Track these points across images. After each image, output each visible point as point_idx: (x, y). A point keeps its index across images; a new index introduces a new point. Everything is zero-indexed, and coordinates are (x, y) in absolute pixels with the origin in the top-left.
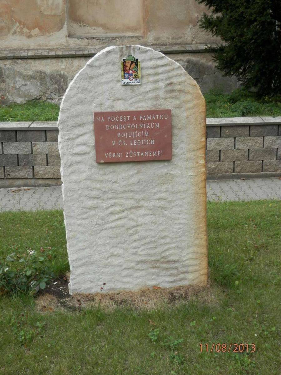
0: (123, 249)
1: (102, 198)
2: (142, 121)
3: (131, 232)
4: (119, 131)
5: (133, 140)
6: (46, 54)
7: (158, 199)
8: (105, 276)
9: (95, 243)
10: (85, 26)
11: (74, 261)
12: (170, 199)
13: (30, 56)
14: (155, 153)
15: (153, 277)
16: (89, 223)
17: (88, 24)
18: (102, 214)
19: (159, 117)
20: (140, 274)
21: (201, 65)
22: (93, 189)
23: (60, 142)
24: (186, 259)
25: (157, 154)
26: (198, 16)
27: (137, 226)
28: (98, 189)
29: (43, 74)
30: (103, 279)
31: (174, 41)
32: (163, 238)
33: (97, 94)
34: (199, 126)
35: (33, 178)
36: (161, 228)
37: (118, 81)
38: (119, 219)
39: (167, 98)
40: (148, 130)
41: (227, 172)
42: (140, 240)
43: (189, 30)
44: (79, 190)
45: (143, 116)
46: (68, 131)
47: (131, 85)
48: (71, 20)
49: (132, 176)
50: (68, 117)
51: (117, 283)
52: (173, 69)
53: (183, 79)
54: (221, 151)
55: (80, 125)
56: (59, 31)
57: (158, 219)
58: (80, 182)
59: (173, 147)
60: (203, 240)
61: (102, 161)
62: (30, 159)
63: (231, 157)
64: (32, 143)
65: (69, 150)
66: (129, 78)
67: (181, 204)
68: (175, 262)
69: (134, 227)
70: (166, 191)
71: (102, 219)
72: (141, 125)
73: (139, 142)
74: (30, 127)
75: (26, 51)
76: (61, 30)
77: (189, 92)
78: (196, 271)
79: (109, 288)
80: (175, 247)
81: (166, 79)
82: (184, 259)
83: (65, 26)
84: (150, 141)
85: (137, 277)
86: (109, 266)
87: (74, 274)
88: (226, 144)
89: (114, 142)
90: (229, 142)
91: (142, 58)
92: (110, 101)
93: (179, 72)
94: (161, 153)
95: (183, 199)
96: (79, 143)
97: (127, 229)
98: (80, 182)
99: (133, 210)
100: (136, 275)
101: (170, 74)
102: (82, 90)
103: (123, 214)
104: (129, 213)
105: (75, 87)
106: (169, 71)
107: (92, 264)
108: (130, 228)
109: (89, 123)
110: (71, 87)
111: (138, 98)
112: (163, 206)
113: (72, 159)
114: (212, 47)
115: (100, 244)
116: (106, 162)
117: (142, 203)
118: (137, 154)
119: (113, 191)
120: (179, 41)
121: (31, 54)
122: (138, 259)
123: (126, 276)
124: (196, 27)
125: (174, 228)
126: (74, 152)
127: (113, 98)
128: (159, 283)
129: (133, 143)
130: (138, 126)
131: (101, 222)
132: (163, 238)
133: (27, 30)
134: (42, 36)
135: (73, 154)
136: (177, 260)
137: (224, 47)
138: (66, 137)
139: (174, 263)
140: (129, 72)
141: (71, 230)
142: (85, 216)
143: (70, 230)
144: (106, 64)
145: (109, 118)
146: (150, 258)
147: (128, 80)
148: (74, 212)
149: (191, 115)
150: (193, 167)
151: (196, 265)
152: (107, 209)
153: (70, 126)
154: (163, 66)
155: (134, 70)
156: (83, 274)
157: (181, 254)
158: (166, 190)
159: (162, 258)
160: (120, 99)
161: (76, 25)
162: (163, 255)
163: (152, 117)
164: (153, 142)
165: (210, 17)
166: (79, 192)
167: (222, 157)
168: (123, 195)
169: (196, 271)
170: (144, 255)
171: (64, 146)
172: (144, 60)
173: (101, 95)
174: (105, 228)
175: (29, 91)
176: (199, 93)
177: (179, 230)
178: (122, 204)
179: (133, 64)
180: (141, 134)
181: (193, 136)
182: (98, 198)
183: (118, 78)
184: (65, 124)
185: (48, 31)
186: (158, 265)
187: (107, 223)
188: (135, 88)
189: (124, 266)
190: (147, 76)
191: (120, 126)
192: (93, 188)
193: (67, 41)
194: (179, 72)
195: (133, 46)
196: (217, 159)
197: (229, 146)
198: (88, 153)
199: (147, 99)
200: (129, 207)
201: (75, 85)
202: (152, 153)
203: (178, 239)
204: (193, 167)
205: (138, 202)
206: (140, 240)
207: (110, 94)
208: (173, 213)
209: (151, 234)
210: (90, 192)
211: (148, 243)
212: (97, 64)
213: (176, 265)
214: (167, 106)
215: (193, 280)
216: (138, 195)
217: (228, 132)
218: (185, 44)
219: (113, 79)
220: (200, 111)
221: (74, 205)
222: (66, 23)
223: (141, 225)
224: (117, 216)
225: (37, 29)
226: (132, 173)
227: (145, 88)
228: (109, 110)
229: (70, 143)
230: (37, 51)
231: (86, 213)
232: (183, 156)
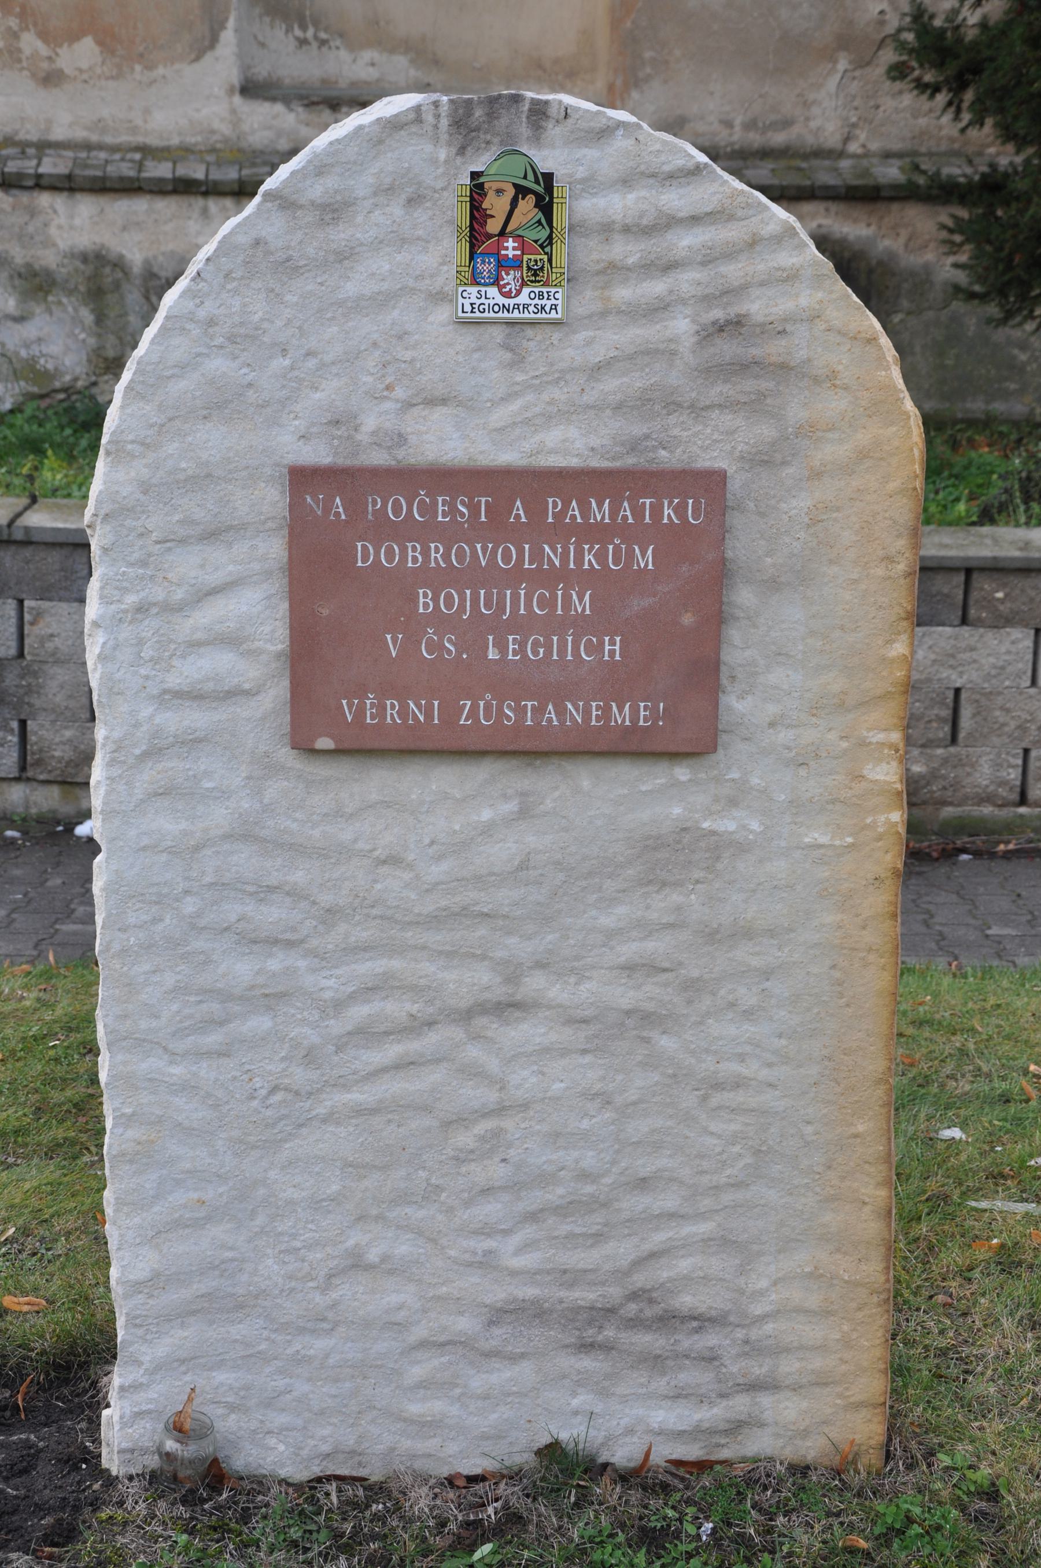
0: (420, 1233)
1: (314, 942)
2: (561, 531)
3: (465, 1139)
4: (428, 577)
5: (500, 629)
6: (127, 170)
7: (629, 968)
8: (309, 1380)
9: (262, 1191)
10: (323, 43)
11: (136, 1287)
12: (695, 973)
13: (51, 175)
14: (621, 710)
15: (575, 1402)
16: (235, 1078)
17: (341, 35)
18: (312, 1036)
19: (657, 511)
20: (500, 1375)
21: (880, 263)
22: (265, 892)
23: (96, 624)
24: (768, 1308)
25: (634, 718)
26: (882, 12)
27: (500, 1110)
28: (295, 894)
29: (107, 270)
30: (295, 1394)
31: (756, 140)
32: (643, 1184)
33: (311, 363)
34: (880, 572)
35: (17, 779)
36: (639, 1127)
37: (440, 297)
38: (403, 1065)
39: (707, 408)
40: (586, 579)
41: (988, 799)
42: (515, 1187)
43: (832, 83)
44: (187, 892)
45: (566, 505)
46: (143, 563)
47: (511, 324)
48: (257, 11)
49: (487, 830)
50: (146, 487)
51: (373, 1421)
52: (753, 243)
53: (806, 298)
54: (964, 695)
55: (212, 535)
56: (197, 59)
57: (619, 1077)
58: (197, 848)
59: (724, 681)
60: (867, 1209)
61: (325, 743)
62: (8, 682)
63: (1013, 724)
64: (21, 602)
65: (143, 671)
66: (496, 282)
67: (753, 1001)
68: (701, 1321)
69: (486, 1114)
70: (671, 926)
71: (310, 1057)
72: (554, 550)
73: (536, 644)
74: (19, 522)
75: (31, 151)
76: (208, 57)
77: (832, 376)
78: (822, 1381)
79: (325, 1448)
80: (707, 1241)
81: (707, 300)
82: (758, 1309)
83: (228, 36)
84: (601, 643)
85: (486, 1397)
86: (336, 1324)
87: (139, 1363)
88: (992, 660)
89: (395, 640)
90: (1009, 652)
91: (581, 172)
92: (388, 405)
93: (786, 259)
94: (654, 716)
95: (767, 974)
96: (199, 635)
97: (447, 1125)
98: (197, 848)
99: (480, 1021)
100: (477, 1382)
101: (733, 271)
102: (232, 339)
103: (430, 1041)
104: (457, 1033)
105: (191, 318)
106: (729, 254)
107: (241, 1307)
108: (460, 1121)
109: (264, 523)
110: (167, 318)
111: (545, 397)
112: (650, 1007)
113: (157, 720)
114: (946, 171)
115: (291, 1202)
116: (346, 745)
117: (535, 983)
118: (521, 711)
119: (374, 912)
120: (779, 139)
121: (55, 165)
122: (498, 1294)
123: (423, 1385)
124: (868, 70)
125: (706, 1131)
126: (173, 681)
127: (399, 393)
128: (608, 1439)
129: (502, 648)
130: (537, 555)
131: (300, 1076)
132: (643, 1184)
133: (39, 44)
134: (112, 78)
135: (165, 691)
136: (714, 1313)
137: (1006, 175)
138: (131, 599)
139: (698, 1330)
140: (499, 247)
141: (133, 1114)
142: (213, 1039)
143: (128, 1111)
144: (375, 194)
145: (374, 503)
146: (563, 1294)
147: (493, 291)
148: (157, 1017)
149: (838, 509)
150: (833, 802)
151: (822, 1348)
152: (339, 1005)
153: (154, 536)
154: (695, 220)
155: (531, 235)
156: (183, 1361)
157: (741, 1281)
158: (671, 919)
159: (634, 1296)
160: (444, 401)
161: (280, 32)
162: (640, 1280)
163: (614, 512)
164: (613, 647)
165: (948, 20)
166: (190, 906)
167: (966, 722)
168: (433, 938)
169: (822, 1381)
170: (532, 1275)
171: (116, 647)
172: (590, 184)
173: (334, 370)
174: (321, 1110)
175: (35, 350)
176: (892, 387)
177: (737, 1149)
178: (423, 982)
179: (527, 205)
180: (548, 603)
181: (842, 628)
182: (290, 944)
183: (440, 281)
184: (128, 522)
185: (141, 55)
186: (609, 1333)
187: (342, 1084)
188: (532, 341)
189: (419, 1332)
190: (598, 273)
191: (436, 552)
192: (271, 889)
193: (233, 111)
194: (786, 259)
195: (530, 94)
196: (941, 735)
197: (1003, 668)
198: (247, 693)
199: (593, 407)
200: (463, 1004)
201: (190, 305)
202: (606, 710)
203: (727, 1198)
204: (833, 802)
205: (513, 979)
206: (515, 1187)
207: (390, 369)
208: (707, 1051)
209: (577, 1161)
210: (250, 908)
211: (562, 1211)
212: (317, 191)
213: (711, 1339)
214: (705, 449)
215: (805, 1433)
216: (512, 940)
217: (1002, 601)
218: (806, 156)
219: (411, 283)
220: (893, 485)
221: (156, 978)
222: (231, 23)
223: (525, 1106)
224: (393, 1051)
225: (87, 46)
226: (486, 815)
227: (589, 343)
228: (378, 458)
229: (149, 627)
230: (83, 155)
231: (221, 1024)
232: (783, 736)
